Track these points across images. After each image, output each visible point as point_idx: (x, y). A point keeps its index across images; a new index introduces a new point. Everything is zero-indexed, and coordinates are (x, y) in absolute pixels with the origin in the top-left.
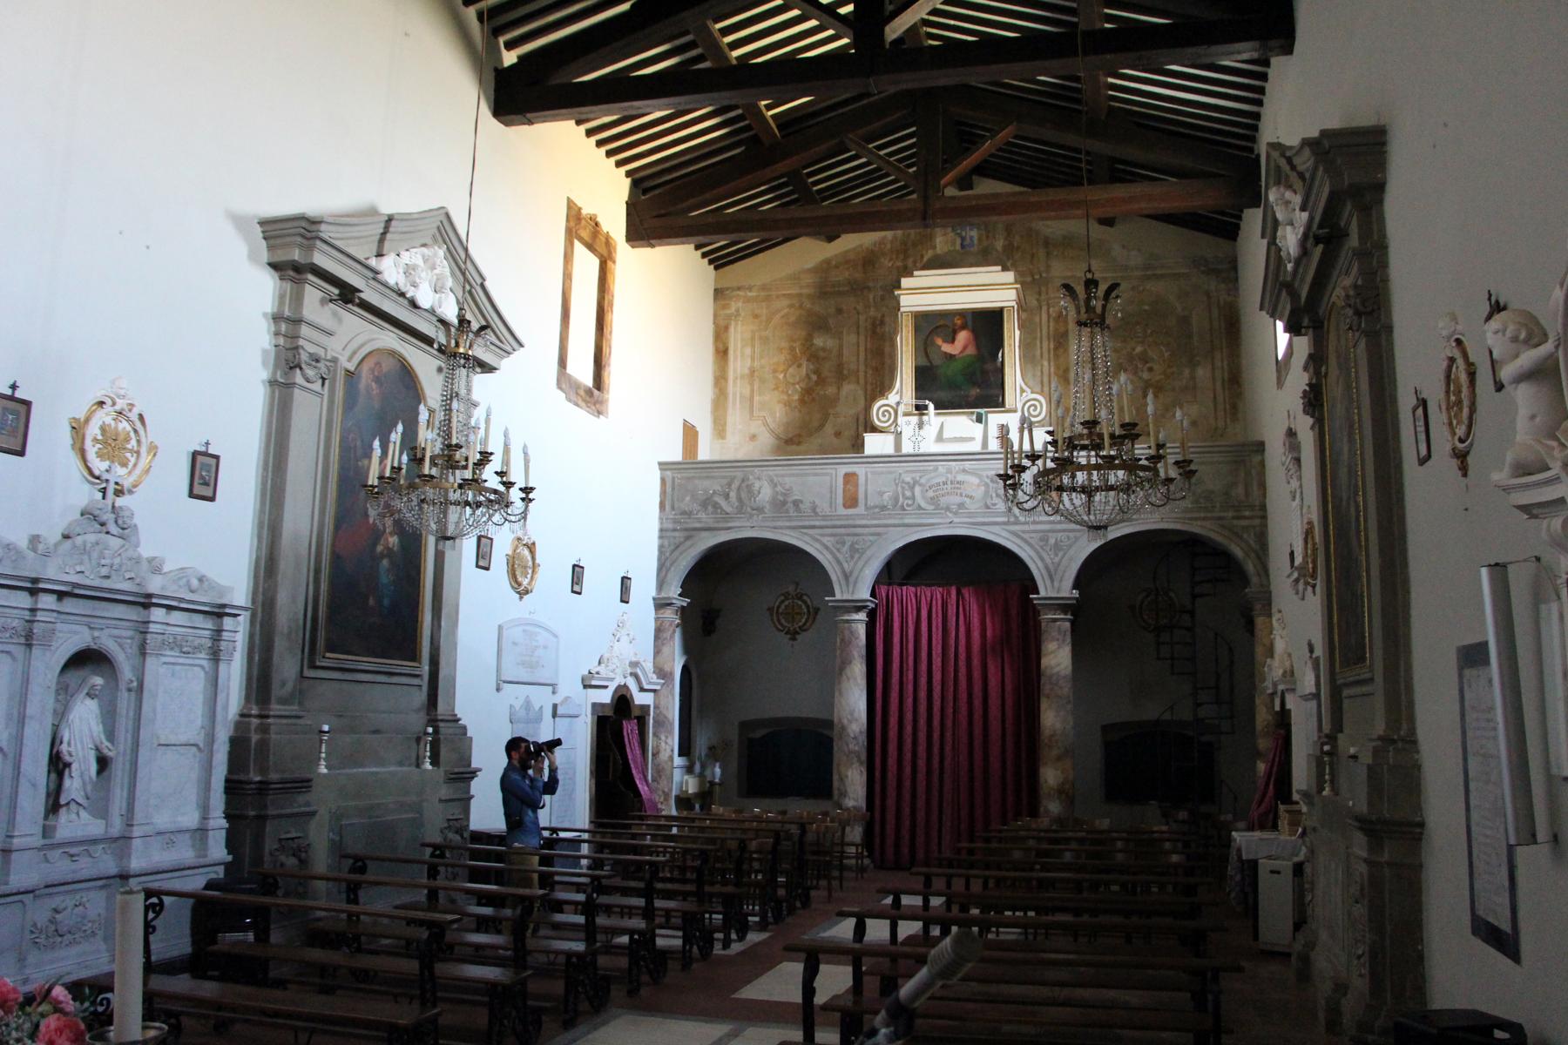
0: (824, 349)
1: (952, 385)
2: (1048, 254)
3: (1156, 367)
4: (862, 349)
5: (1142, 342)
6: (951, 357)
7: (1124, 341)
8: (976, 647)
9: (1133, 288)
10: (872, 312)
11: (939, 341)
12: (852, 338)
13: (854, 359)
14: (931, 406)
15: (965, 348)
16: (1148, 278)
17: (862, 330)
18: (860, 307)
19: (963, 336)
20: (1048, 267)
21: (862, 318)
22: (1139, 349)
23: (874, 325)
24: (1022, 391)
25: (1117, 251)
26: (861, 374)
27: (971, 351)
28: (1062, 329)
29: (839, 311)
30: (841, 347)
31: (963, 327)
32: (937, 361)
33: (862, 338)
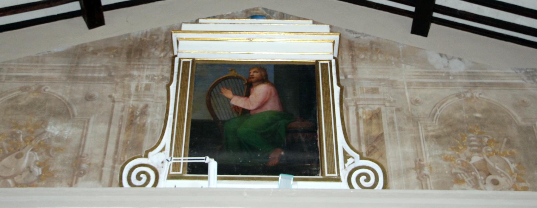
0: (59, 139)
1: (243, 145)
2: (353, 59)
3: (501, 180)
4: (113, 140)
5: (479, 152)
6: (245, 112)
7: (456, 148)
8: (499, 71)
9: (458, 95)
10: (132, 102)
11: (228, 94)
12: (102, 128)
13: (99, 151)
14: (213, 165)
15: (263, 104)
16: (475, 86)
17: (115, 120)
18: (116, 96)
19: (261, 91)
20: (354, 69)
21: (118, 107)
22: (476, 159)
23: (132, 116)
24: (346, 157)
25: (434, 59)
26: (107, 170)
27: (273, 106)
28: (375, 133)
29: (89, 98)
30: (84, 137)
31: (263, 80)
32: (223, 115)
33: (114, 129)
